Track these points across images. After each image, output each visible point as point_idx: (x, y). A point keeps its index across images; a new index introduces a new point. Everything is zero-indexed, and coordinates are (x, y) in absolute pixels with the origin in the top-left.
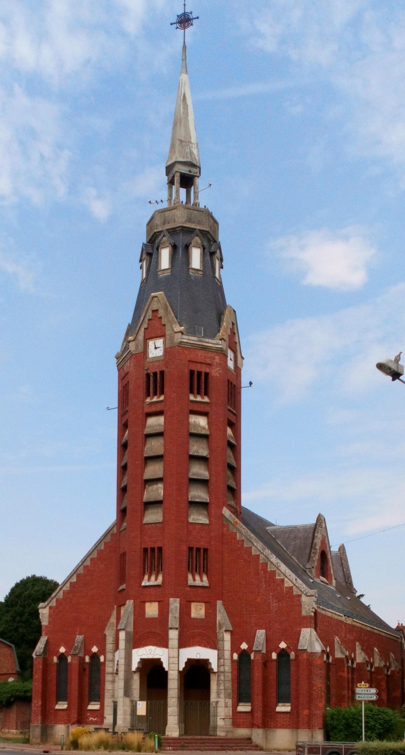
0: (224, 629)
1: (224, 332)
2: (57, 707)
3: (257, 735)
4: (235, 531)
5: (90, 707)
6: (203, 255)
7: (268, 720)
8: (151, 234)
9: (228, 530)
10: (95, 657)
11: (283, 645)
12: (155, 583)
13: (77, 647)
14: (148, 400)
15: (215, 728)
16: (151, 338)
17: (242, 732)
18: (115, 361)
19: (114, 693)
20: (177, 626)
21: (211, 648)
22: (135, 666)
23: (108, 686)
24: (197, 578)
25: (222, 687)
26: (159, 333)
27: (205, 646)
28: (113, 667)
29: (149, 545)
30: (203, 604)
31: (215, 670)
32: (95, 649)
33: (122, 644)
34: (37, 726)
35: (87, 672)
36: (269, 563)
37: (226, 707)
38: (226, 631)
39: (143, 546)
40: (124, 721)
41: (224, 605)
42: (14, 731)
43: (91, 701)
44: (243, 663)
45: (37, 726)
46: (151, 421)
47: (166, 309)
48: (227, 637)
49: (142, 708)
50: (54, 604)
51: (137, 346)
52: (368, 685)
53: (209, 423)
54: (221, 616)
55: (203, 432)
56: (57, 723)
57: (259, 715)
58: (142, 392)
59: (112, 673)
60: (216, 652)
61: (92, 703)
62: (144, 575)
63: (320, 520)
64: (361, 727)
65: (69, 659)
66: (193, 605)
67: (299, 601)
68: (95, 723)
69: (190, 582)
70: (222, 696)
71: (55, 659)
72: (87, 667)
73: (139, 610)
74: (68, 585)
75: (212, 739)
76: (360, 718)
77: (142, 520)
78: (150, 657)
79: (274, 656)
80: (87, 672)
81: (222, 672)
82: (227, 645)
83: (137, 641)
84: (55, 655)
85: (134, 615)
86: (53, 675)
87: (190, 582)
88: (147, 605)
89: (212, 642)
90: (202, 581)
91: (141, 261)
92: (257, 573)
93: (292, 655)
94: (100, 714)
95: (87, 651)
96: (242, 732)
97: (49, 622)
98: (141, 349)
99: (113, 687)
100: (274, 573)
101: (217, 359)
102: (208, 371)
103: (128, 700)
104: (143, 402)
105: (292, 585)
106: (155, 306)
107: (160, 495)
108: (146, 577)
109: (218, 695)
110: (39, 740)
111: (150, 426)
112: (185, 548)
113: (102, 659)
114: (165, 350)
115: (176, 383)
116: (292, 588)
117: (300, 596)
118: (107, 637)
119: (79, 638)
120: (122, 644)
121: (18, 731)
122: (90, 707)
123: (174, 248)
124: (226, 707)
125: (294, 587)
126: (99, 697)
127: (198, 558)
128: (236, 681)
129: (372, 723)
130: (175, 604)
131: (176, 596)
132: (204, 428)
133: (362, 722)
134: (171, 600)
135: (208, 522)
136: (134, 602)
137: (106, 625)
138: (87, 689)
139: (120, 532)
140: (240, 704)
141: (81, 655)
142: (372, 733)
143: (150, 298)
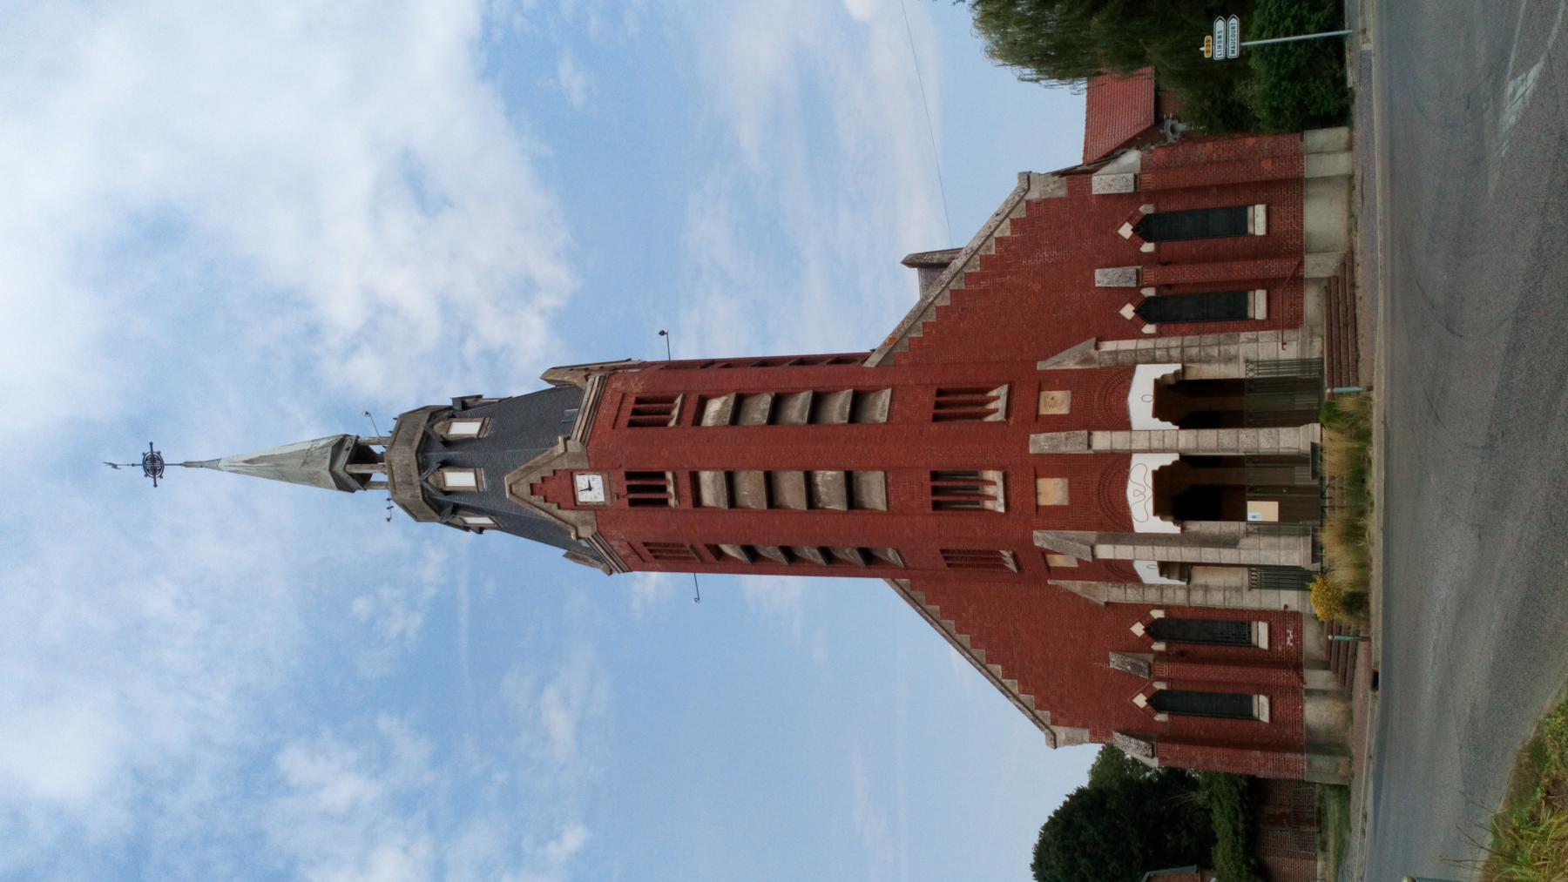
0: (1093, 351)
1: (577, 380)
2: (1265, 718)
3: (1318, 266)
4: (906, 341)
5: (1263, 643)
6: (463, 418)
7: (1287, 245)
8: (428, 509)
9: (905, 355)
10: (1154, 630)
11: (1126, 231)
12: (1000, 484)
13: (1134, 666)
14: (672, 502)
15: (1304, 363)
16: (575, 497)
17: (1312, 303)
18: (615, 574)
19: (1231, 588)
20: (1085, 432)
21: (1131, 378)
22: (1169, 527)
23: (1216, 600)
24: (992, 406)
25: (1214, 352)
26: (566, 482)
27: (1128, 388)
28: (1174, 587)
29: (929, 498)
30: (1044, 394)
31: (1178, 367)
32: (1138, 629)
33: (1122, 552)
34: (1309, 762)
35: (1188, 647)
36: (966, 270)
37: (1257, 340)
38: (1097, 347)
39: (929, 510)
40: (1292, 553)
41: (1045, 358)
42: (1320, 864)
43: (1250, 642)
44: (1164, 312)
45: (1309, 762)
46: (708, 498)
47: (530, 469)
48: (1109, 346)
49: (1262, 511)
50: (1048, 713)
51: (585, 523)
52: (1208, 38)
53: (717, 396)
54: (1068, 361)
55: (731, 403)
56: (1300, 720)
57: (1273, 267)
58: (658, 514)
59: (1189, 591)
60: (1140, 368)
61: (1254, 640)
62: (983, 510)
63: (911, 262)
64: (1300, 42)
65: (1160, 686)
66: (1043, 411)
67: (1038, 204)
68: (1299, 632)
69: (998, 417)
70: (1232, 350)
71: (1161, 717)
72: (1176, 648)
73: (1055, 518)
74: (1008, 682)
75: (1331, 369)
76: (1278, 49)
77: (881, 513)
78: (1149, 493)
79: (1148, 248)
80: (1188, 647)
81: (1182, 352)
82: (1127, 345)
83: (1118, 524)
84: (1152, 716)
85: (1063, 528)
86: (1196, 724)
87: (998, 417)
88: (1043, 501)
89: (1122, 375)
90: (998, 398)
91: (466, 528)
92: (985, 292)
93: (1146, 209)
94: (1280, 620)
95: (1141, 646)
96: (1312, 303)
97: (1085, 726)
98: (589, 516)
99: (1218, 589)
100: (985, 260)
101: (617, 384)
102: (633, 400)
103: (1244, 542)
104: (672, 510)
105: (1007, 221)
106: (524, 490)
107: (836, 478)
108: (989, 505)
109: (1230, 359)
110: (1342, 760)
111: (717, 500)
112: (935, 427)
113: (1158, 614)
114: (594, 470)
115: (650, 451)
116: (1013, 222)
117: (1028, 203)
118: (1112, 600)
119: (1115, 661)
120: (1122, 552)
121: (1320, 857)
122: (1263, 643)
123: (446, 464)
124: (1257, 340)
125: (1012, 216)
126: (1236, 625)
127: (955, 404)
128: (1201, 325)
129: (1288, 22)
130: (1040, 443)
131: (1025, 443)
132: (725, 403)
133: (1286, 43)
134: (1032, 450)
135: (889, 391)
136: (1038, 529)
137: (1087, 600)
138: (1227, 723)
139: (906, 567)
140: (1251, 314)
141: (1150, 658)
142: (1309, 23)
143: (514, 499)
